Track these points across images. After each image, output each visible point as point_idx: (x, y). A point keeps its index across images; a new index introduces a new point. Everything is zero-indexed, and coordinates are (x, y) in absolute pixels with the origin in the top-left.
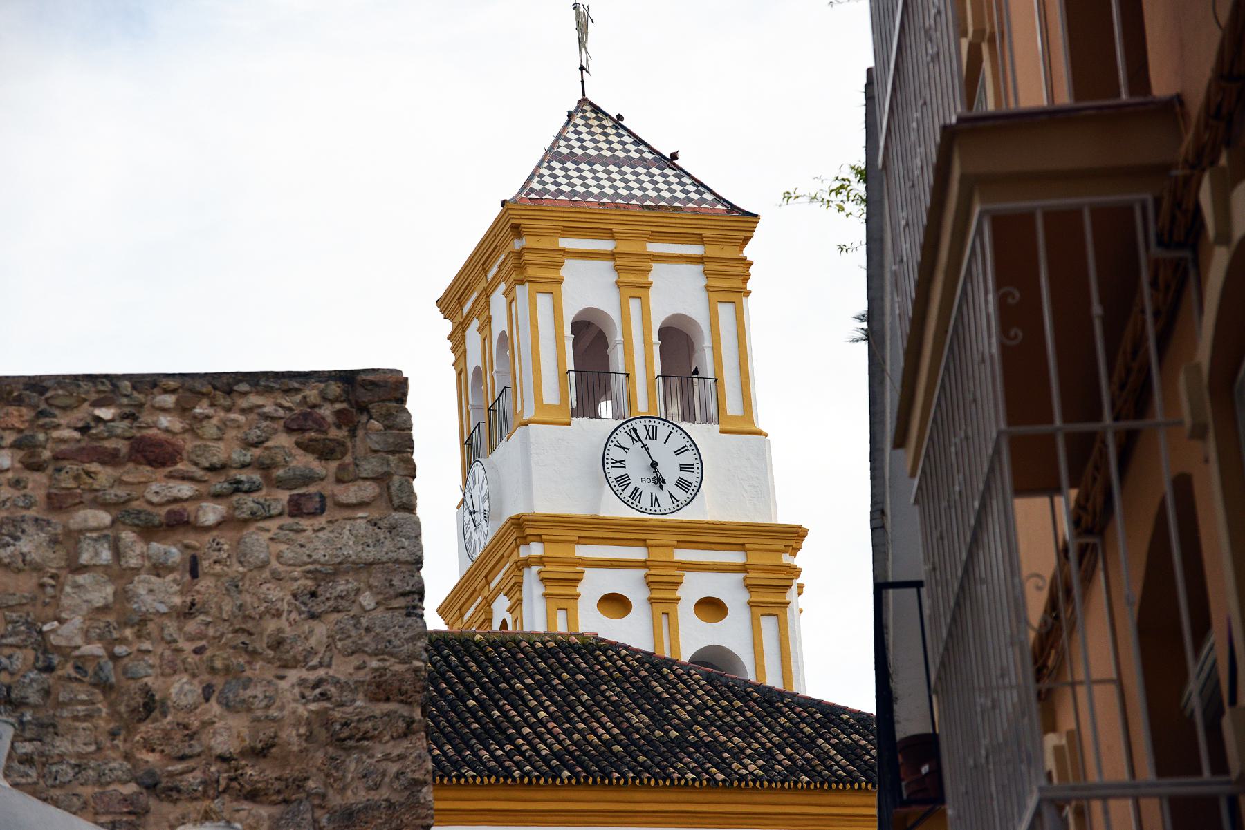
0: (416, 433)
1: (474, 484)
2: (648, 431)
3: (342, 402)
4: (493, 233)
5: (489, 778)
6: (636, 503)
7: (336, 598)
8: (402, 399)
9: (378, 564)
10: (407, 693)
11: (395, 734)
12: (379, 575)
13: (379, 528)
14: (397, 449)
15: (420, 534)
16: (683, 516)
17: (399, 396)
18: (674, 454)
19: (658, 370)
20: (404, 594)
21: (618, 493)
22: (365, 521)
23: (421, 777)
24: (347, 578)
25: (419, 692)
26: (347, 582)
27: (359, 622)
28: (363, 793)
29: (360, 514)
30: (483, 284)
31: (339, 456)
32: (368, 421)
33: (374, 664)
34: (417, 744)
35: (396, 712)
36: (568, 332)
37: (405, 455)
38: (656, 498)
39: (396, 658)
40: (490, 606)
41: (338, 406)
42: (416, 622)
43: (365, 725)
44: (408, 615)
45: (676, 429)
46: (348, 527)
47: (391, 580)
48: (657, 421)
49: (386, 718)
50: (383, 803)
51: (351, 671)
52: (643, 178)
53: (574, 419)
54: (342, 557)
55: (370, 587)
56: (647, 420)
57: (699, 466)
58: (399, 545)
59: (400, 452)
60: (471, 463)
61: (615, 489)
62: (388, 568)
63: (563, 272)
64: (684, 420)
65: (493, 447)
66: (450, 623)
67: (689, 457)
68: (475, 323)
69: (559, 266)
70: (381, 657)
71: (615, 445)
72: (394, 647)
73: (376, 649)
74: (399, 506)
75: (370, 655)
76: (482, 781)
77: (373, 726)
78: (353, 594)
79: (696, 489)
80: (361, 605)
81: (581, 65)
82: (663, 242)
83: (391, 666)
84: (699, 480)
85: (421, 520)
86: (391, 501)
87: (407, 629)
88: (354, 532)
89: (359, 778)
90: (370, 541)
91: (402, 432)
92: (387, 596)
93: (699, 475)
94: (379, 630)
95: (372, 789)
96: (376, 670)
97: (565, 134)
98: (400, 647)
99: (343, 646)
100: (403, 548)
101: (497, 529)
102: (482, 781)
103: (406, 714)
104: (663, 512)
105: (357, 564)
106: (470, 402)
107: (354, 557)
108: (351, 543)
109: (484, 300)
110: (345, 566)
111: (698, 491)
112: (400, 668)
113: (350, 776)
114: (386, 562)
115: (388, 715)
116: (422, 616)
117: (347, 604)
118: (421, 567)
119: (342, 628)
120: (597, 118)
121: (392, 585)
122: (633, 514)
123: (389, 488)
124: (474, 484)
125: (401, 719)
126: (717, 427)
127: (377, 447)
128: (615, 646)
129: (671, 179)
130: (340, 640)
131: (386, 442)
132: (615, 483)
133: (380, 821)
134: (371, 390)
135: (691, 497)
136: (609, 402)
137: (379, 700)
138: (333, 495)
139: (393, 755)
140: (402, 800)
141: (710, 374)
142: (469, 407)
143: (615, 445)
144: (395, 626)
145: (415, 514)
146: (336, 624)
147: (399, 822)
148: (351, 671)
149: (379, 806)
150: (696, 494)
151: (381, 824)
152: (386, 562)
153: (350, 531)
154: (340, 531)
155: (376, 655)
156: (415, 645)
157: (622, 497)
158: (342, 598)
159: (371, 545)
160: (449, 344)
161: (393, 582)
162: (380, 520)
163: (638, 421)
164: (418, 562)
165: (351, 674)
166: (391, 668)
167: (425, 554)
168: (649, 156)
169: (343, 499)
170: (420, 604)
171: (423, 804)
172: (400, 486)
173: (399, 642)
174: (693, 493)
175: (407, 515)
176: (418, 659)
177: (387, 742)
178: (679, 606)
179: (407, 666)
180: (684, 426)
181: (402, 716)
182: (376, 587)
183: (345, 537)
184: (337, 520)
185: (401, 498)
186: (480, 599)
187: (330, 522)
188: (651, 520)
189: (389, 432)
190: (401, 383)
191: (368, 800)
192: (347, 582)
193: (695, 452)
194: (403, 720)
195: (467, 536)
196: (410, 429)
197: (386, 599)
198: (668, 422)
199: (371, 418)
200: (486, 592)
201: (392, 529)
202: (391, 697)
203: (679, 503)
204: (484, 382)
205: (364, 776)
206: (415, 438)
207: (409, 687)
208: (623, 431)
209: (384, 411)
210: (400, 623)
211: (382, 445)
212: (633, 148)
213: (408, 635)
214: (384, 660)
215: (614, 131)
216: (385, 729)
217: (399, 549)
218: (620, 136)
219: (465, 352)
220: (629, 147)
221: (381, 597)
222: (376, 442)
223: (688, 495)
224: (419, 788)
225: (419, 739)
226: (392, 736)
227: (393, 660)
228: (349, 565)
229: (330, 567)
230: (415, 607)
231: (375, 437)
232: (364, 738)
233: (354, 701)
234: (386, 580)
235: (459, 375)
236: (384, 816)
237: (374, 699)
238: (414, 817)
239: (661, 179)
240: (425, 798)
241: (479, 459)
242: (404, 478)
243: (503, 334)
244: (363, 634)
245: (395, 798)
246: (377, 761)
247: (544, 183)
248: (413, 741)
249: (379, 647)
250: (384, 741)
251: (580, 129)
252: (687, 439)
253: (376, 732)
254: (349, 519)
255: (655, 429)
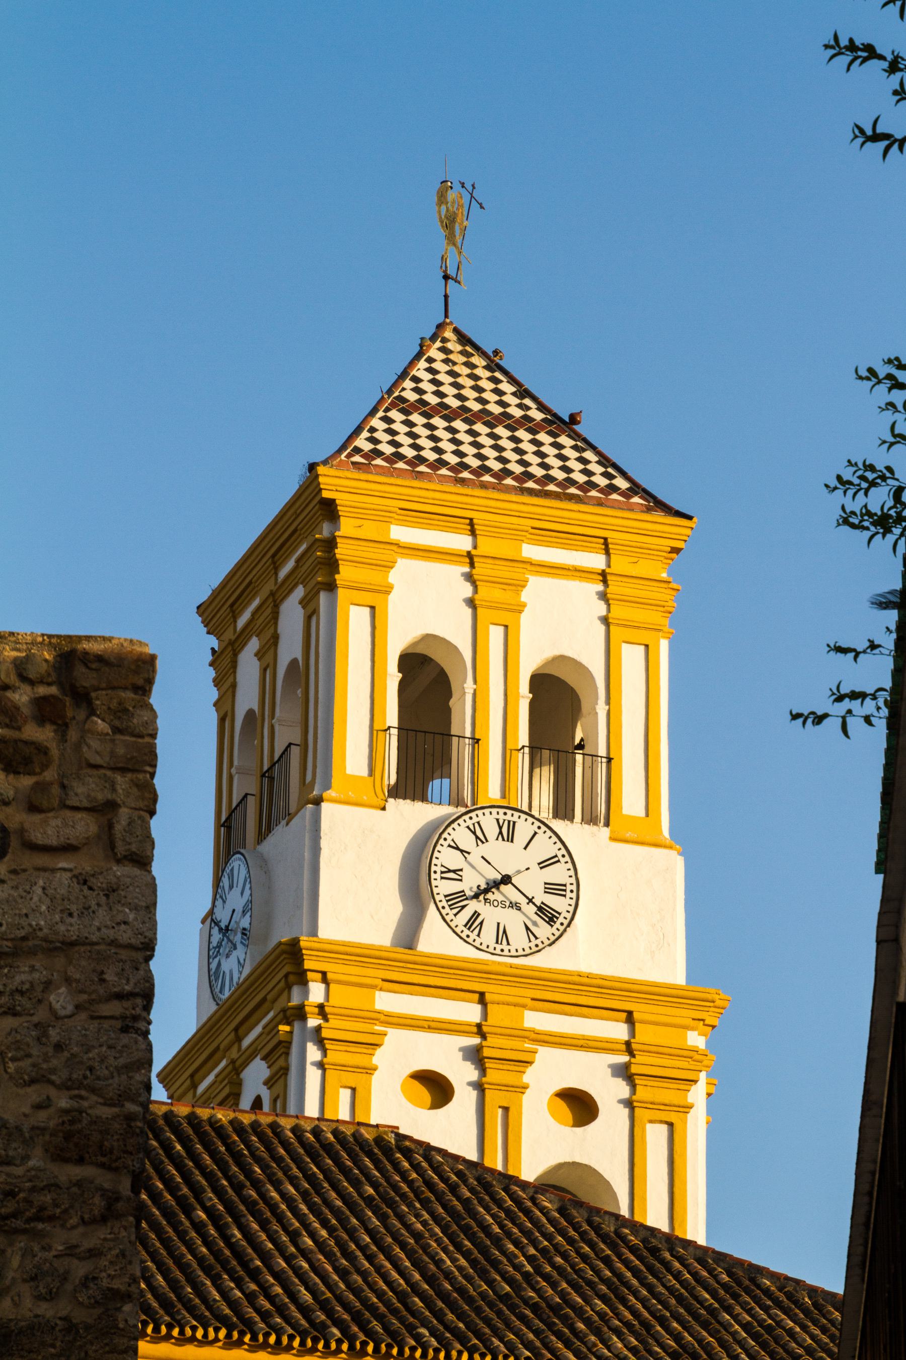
0: (162, 744)
1: (231, 887)
2: (500, 828)
3: (49, 684)
4: (292, 511)
5: (217, 1330)
6: (473, 936)
7: (12, 994)
8: (144, 688)
9: (84, 944)
10: (111, 1152)
11: (86, 1216)
12: (83, 963)
13: (90, 888)
14: (130, 766)
15: (155, 904)
16: (545, 960)
17: (140, 682)
18: (538, 867)
19: (523, 739)
20: (120, 996)
21: (448, 918)
22: (69, 874)
23: (123, 1288)
24: (32, 962)
25: (131, 1153)
26: (33, 968)
27: (45, 1034)
28: (28, 1302)
29: (63, 864)
30: (270, 586)
31: (37, 770)
32: (88, 718)
33: (64, 1103)
34: (121, 1236)
35: (92, 1182)
36: (393, 678)
37: (141, 776)
38: (505, 932)
39: (100, 1096)
40: (238, 1074)
41: (42, 690)
42: (136, 1042)
43: (42, 1198)
44: (125, 1030)
45: (544, 828)
46: (41, 883)
47: (102, 973)
48: (516, 814)
49: (75, 1189)
50: (58, 1322)
51: (26, 1110)
52: (526, 446)
53: (391, 800)
54: (28, 929)
55: (68, 980)
56: (502, 811)
57: (574, 888)
58: (120, 918)
59: (134, 771)
60: (228, 856)
61: (444, 912)
62: (98, 952)
63: (393, 577)
64: (556, 815)
65: (263, 834)
66: (176, 1095)
67: (559, 874)
68: (254, 644)
69: (389, 566)
70: (76, 1092)
71: (449, 846)
72: (98, 1078)
73: (70, 1079)
74: (125, 857)
75: (58, 1087)
76: (205, 1335)
77: (54, 1200)
78: (40, 988)
79: (566, 922)
80: (51, 1007)
81: (445, 271)
82: (549, 544)
83: (90, 1107)
84: (571, 909)
85: (158, 882)
86: (112, 846)
87: (121, 1052)
88: (50, 891)
89: (25, 1281)
90: (74, 908)
91: (140, 740)
92: (94, 996)
93: (573, 902)
94: (75, 1049)
95: (45, 1299)
96: (67, 1111)
97: (414, 372)
98: (106, 1079)
99: (17, 1070)
100: (125, 923)
101: (259, 959)
102: (205, 1335)
103: (106, 1185)
104: (513, 953)
105: (51, 942)
106: (236, 763)
107: (45, 931)
108: (44, 908)
109: (269, 610)
110: (30, 943)
111: (569, 925)
112: (106, 1112)
113: (10, 1275)
114: (97, 944)
115: (79, 1184)
116: (147, 1032)
117: (28, 1005)
118: (151, 957)
119: (17, 1041)
120: (463, 353)
121: (102, 981)
122: (470, 953)
123: (111, 826)
124: (231, 887)
125: (99, 1193)
126: (605, 832)
127: (98, 760)
128: (428, 1149)
129: (567, 452)
130: (13, 1059)
131: (112, 754)
132: (444, 903)
133: (52, 1350)
134: (96, 670)
135: (557, 934)
136: (446, 781)
137: (66, 1160)
138: (22, 831)
139: (82, 1249)
140: (90, 1321)
141: (602, 751)
142: (233, 771)
143: (449, 846)
144: (101, 1046)
145: (150, 872)
146: (9, 1034)
147: (83, 1354)
148: (26, 1110)
149: (53, 1328)
150: (565, 930)
151: (52, 1355)
152: (97, 944)
153: (44, 889)
154: (28, 888)
155: (68, 1089)
156: (130, 1078)
157: (453, 924)
158: (22, 993)
159: (75, 914)
160: (211, 673)
161: (106, 977)
162: (93, 875)
163: (487, 811)
164: (148, 948)
165: (25, 1115)
166: (89, 1111)
167: (159, 936)
168: (538, 416)
169: (38, 838)
170: (144, 1014)
171: (123, 1330)
172: (129, 824)
173: (106, 1072)
174: (562, 928)
175: (136, 871)
176: (133, 1101)
177: (73, 1227)
178: (525, 1098)
179: (116, 1110)
180: (557, 825)
181: (101, 1189)
182: (78, 981)
183: (36, 899)
184: (25, 870)
185: (130, 844)
186: (224, 1063)
187: (14, 872)
188: (494, 962)
189: (118, 737)
190: (144, 662)
191: (37, 1316)
192: (33, 968)
193: (570, 865)
194: (102, 1196)
195: (214, 966)
196: (154, 736)
197: (91, 1002)
198: (533, 816)
199: (92, 712)
200: (234, 1053)
201: (111, 891)
202: (87, 1156)
203: (538, 942)
204: (259, 730)
205: (34, 1278)
206: (159, 751)
207: (115, 1144)
208: (463, 825)
209: (114, 705)
210: (111, 1042)
211: (107, 759)
212: (513, 401)
213: (122, 1061)
214: (81, 1097)
215: (488, 374)
216: (71, 1207)
217: (118, 924)
218: (496, 381)
219: (234, 686)
220: (508, 399)
221: (85, 997)
222: (97, 753)
223: (554, 930)
224: (119, 1305)
225: (125, 1228)
226: (82, 1219)
227: (94, 1098)
228: (37, 942)
229: (9, 944)
230: (136, 1018)
231: (95, 744)
232: (37, 1218)
233: (26, 1158)
234: (94, 971)
235: (222, 720)
236: (58, 1344)
237: (59, 1156)
238: (107, 1349)
239: (552, 451)
240: (126, 1321)
241: (242, 851)
242: (137, 812)
243: (294, 663)
244: (50, 1054)
245: (80, 1316)
246: (55, 1256)
247: (374, 441)
248: (116, 1230)
249: (75, 1076)
250: (68, 1226)
251: (437, 366)
252: (559, 845)
253: (58, 1211)
254: (44, 870)
255: (512, 826)
